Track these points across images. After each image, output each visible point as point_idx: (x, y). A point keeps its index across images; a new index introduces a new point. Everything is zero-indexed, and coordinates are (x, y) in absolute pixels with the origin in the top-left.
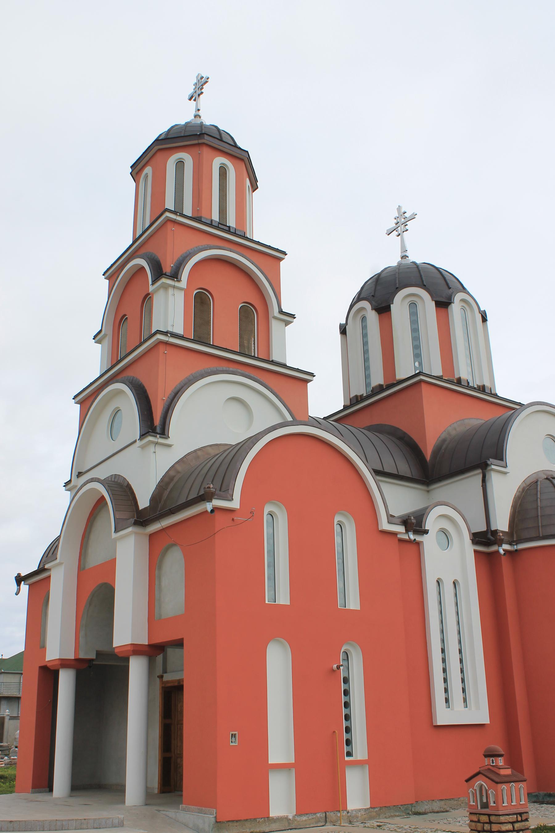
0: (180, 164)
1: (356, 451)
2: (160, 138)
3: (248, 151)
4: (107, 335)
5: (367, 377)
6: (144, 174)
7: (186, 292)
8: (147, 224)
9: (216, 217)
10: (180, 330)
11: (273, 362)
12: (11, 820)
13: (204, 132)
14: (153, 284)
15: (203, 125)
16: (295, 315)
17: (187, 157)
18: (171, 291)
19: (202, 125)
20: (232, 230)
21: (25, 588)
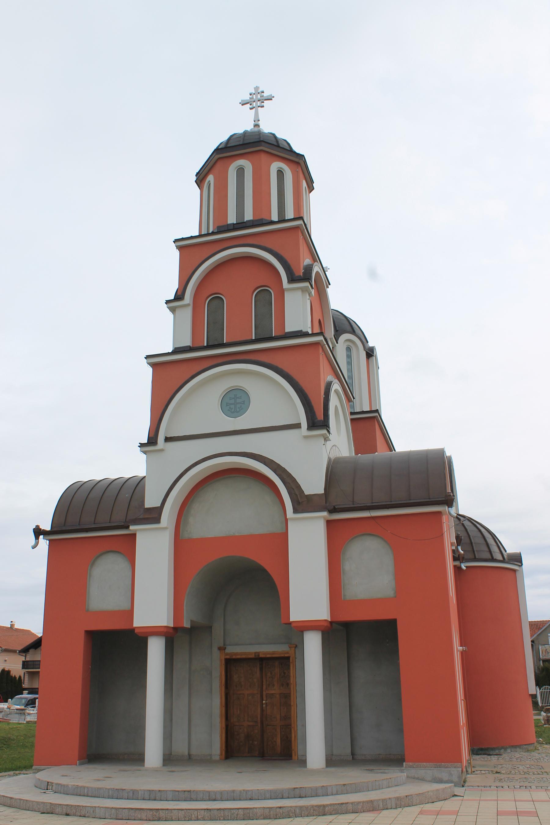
0: (241, 171)
2: (220, 147)
3: (305, 156)
6: (208, 181)
12: (344, 783)
13: (262, 140)
15: (261, 133)
19: (260, 133)
21: (44, 543)
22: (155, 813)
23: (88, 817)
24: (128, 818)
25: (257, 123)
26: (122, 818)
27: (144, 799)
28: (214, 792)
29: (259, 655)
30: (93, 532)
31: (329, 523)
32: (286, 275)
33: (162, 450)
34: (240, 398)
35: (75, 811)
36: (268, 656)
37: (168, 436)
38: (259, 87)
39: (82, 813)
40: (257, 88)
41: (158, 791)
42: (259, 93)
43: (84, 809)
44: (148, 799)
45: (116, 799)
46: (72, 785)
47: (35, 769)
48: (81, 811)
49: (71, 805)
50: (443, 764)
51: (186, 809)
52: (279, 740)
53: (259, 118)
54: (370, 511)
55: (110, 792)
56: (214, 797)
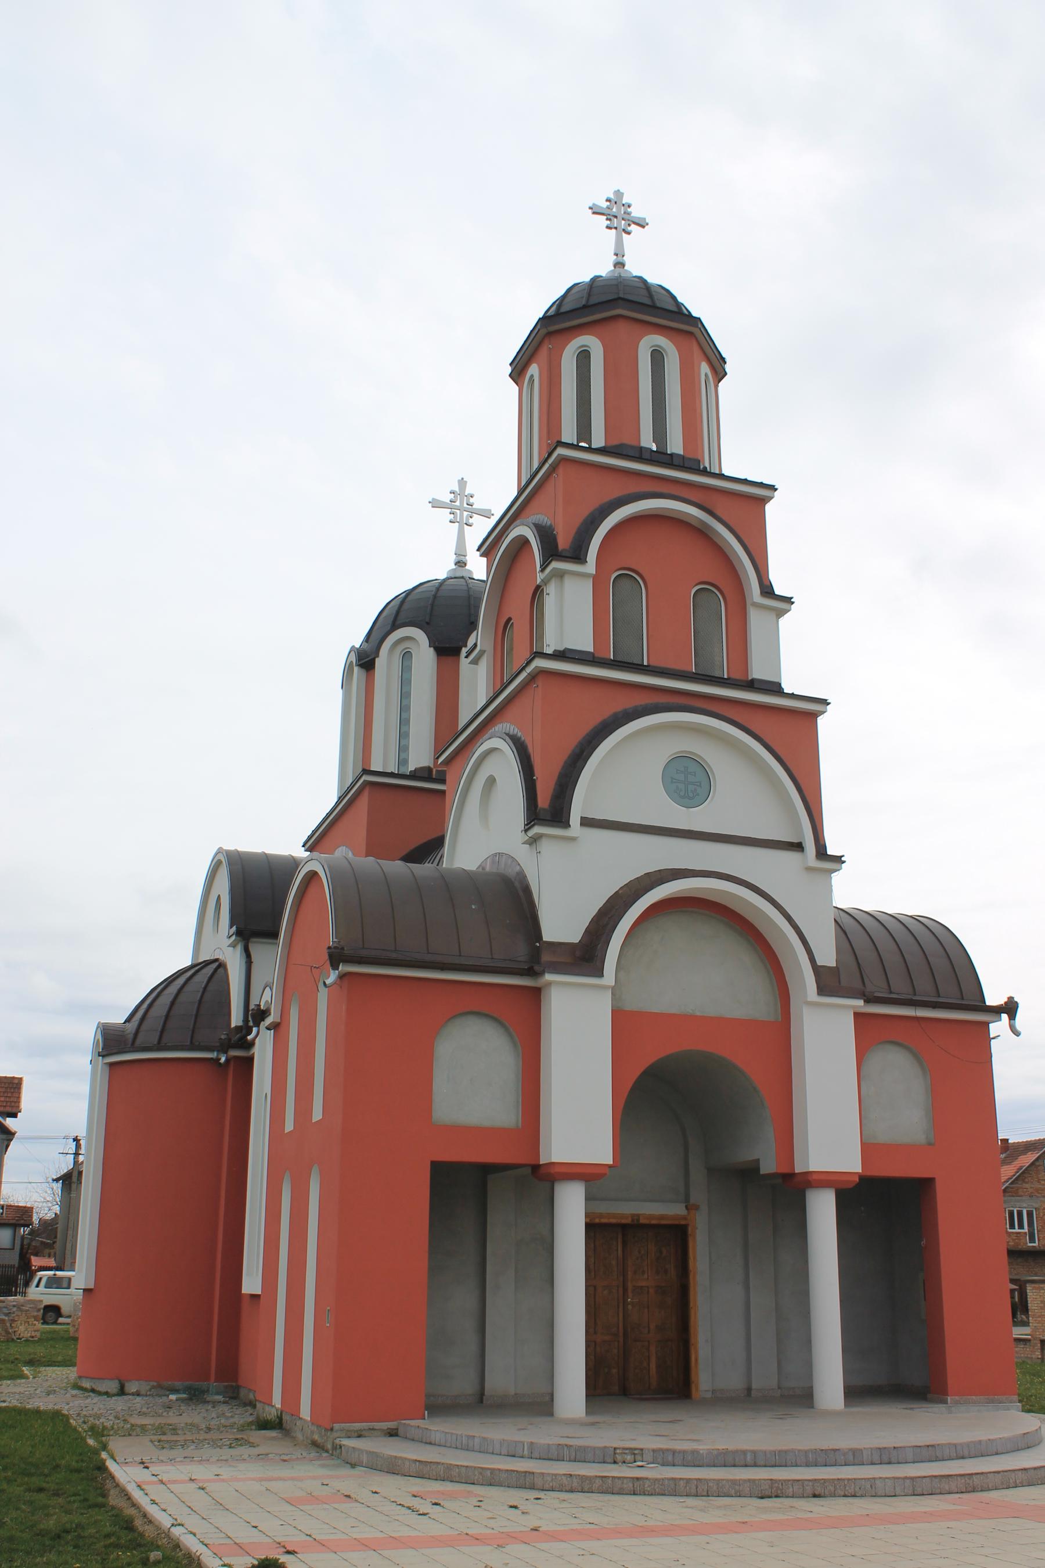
0: (584, 357)
1: (471, 754)
4: (485, 651)
5: (403, 749)
7: (598, 582)
8: (536, 465)
9: (648, 441)
10: (585, 643)
11: (752, 685)
14: (542, 570)
16: (792, 598)
17: (592, 342)
18: (568, 582)
20: (676, 462)
22: (968, 1481)
23: (862, 1496)
24: (930, 1492)
25: (620, 259)
26: (922, 1493)
27: (872, 1464)
28: (961, 1444)
29: (638, 1220)
30: (456, 972)
31: (859, 1017)
32: (757, 580)
33: (573, 839)
34: (694, 774)
35: (832, 1489)
36: (654, 1222)
37: (583, 816)
38: (623, 194)
39: (847, 1490)
40: (619, 194)
41: (893, 1448)
42: (623, 205)
43: (853, 1484)
44: (880, 1462)
45: (824, 1466)
46: (708, 1449)
47: (341, 1430)
48: (845, 1488)
49: (823, 1479)
50: (996, 1397)
51: (1003, 1471)
52: (653, 1366)
53: (624, 251)
54: (917, 1008)
55: (810, 1456)
56: (961, 1452)
